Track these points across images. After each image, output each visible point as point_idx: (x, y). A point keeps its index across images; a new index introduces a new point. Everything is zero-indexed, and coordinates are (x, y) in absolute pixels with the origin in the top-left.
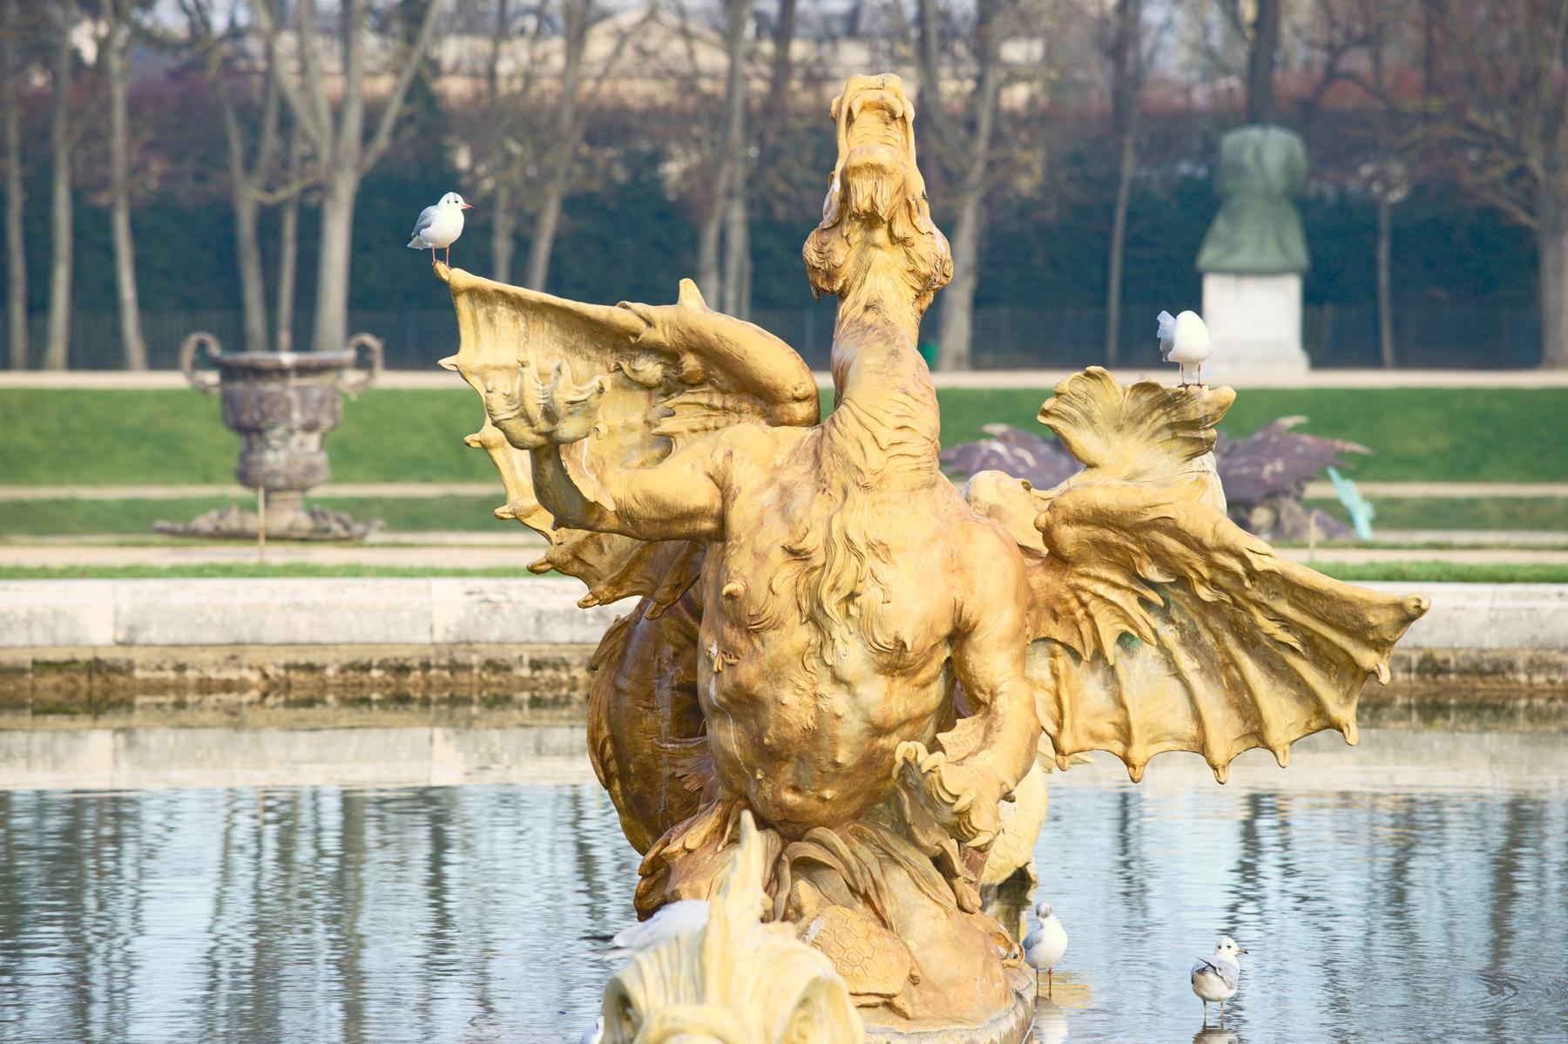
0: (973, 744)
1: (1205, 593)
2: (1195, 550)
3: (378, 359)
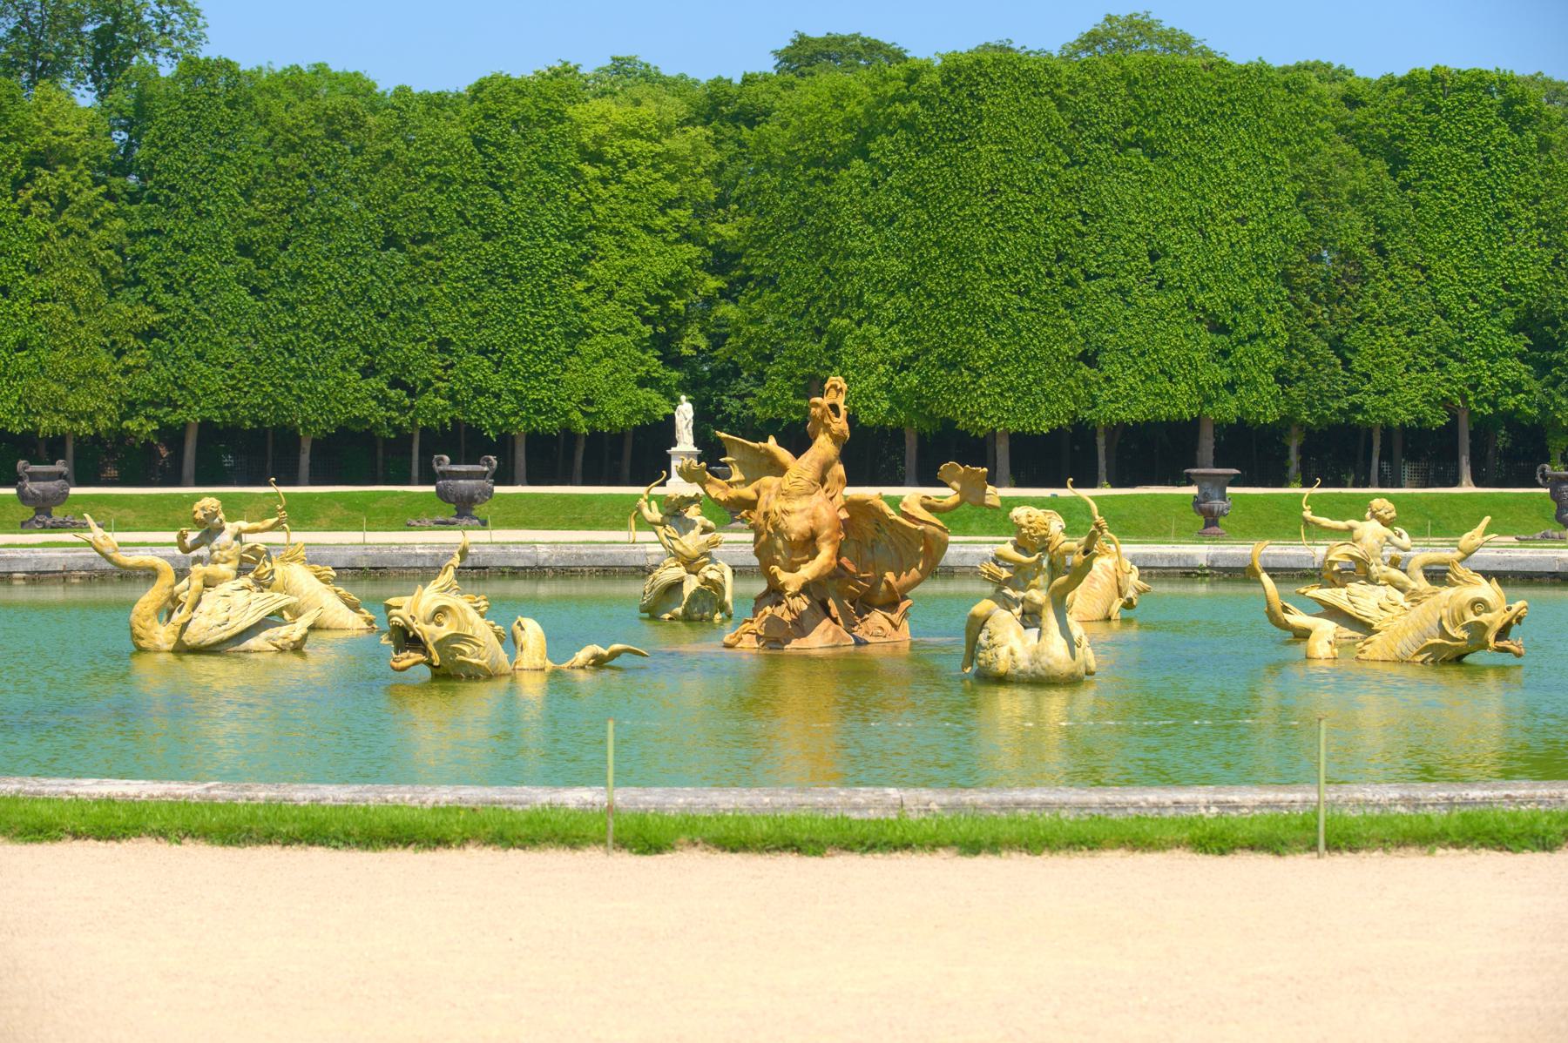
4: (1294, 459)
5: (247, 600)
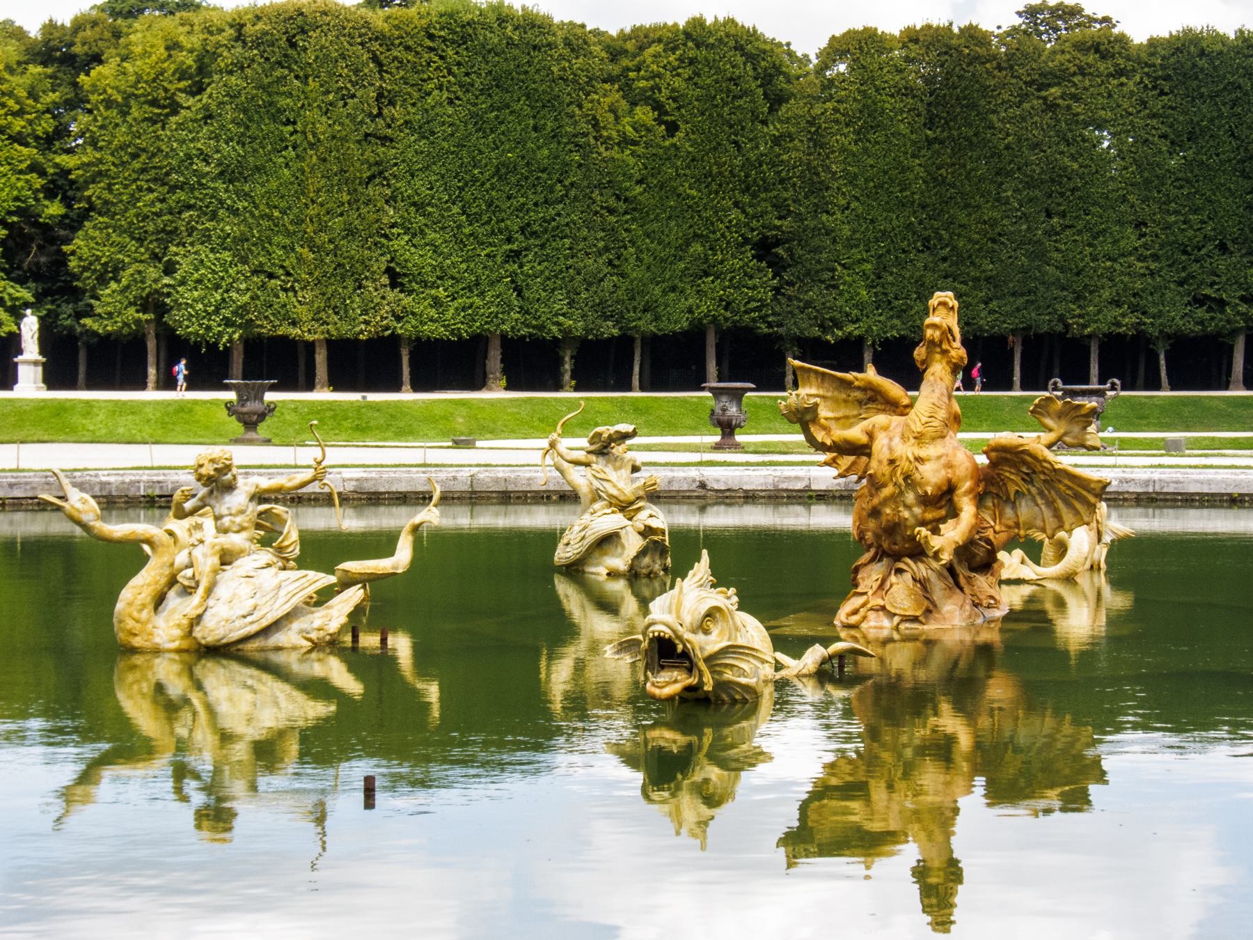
3: (1119, 387)
5: (276, 581)
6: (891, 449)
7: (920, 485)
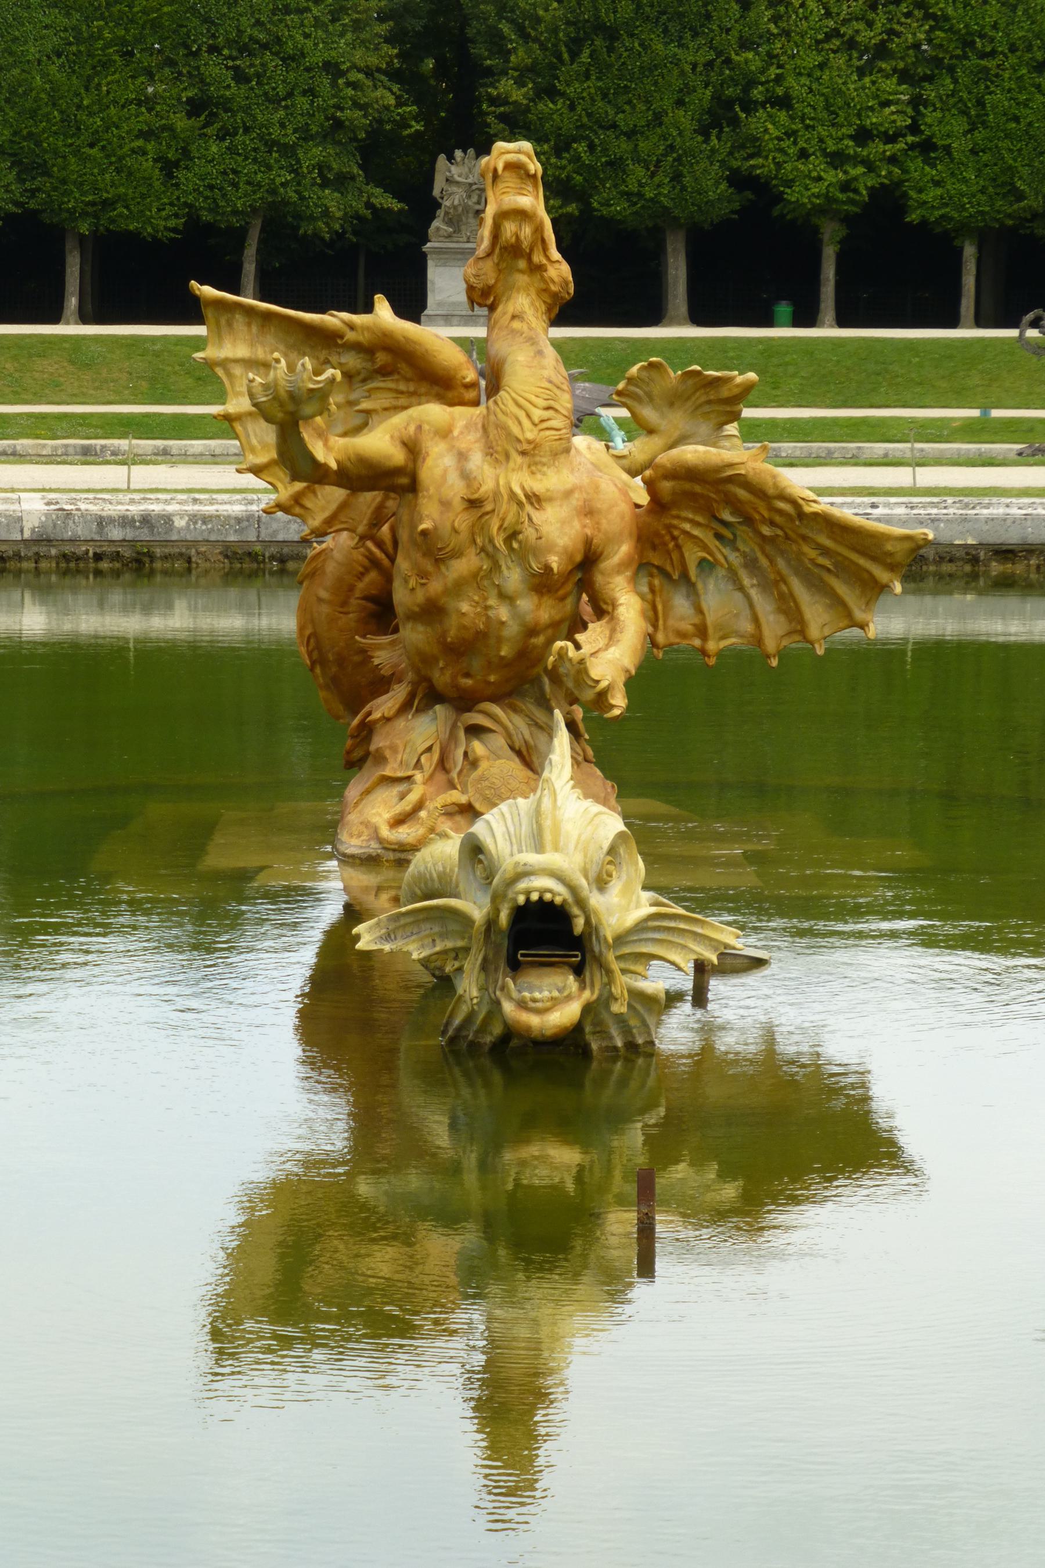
0: (601, 643)
1: (766, 531)
2: (759, 497)
4: (72, 302)
6: (466, 476)
7: (536, 551)
